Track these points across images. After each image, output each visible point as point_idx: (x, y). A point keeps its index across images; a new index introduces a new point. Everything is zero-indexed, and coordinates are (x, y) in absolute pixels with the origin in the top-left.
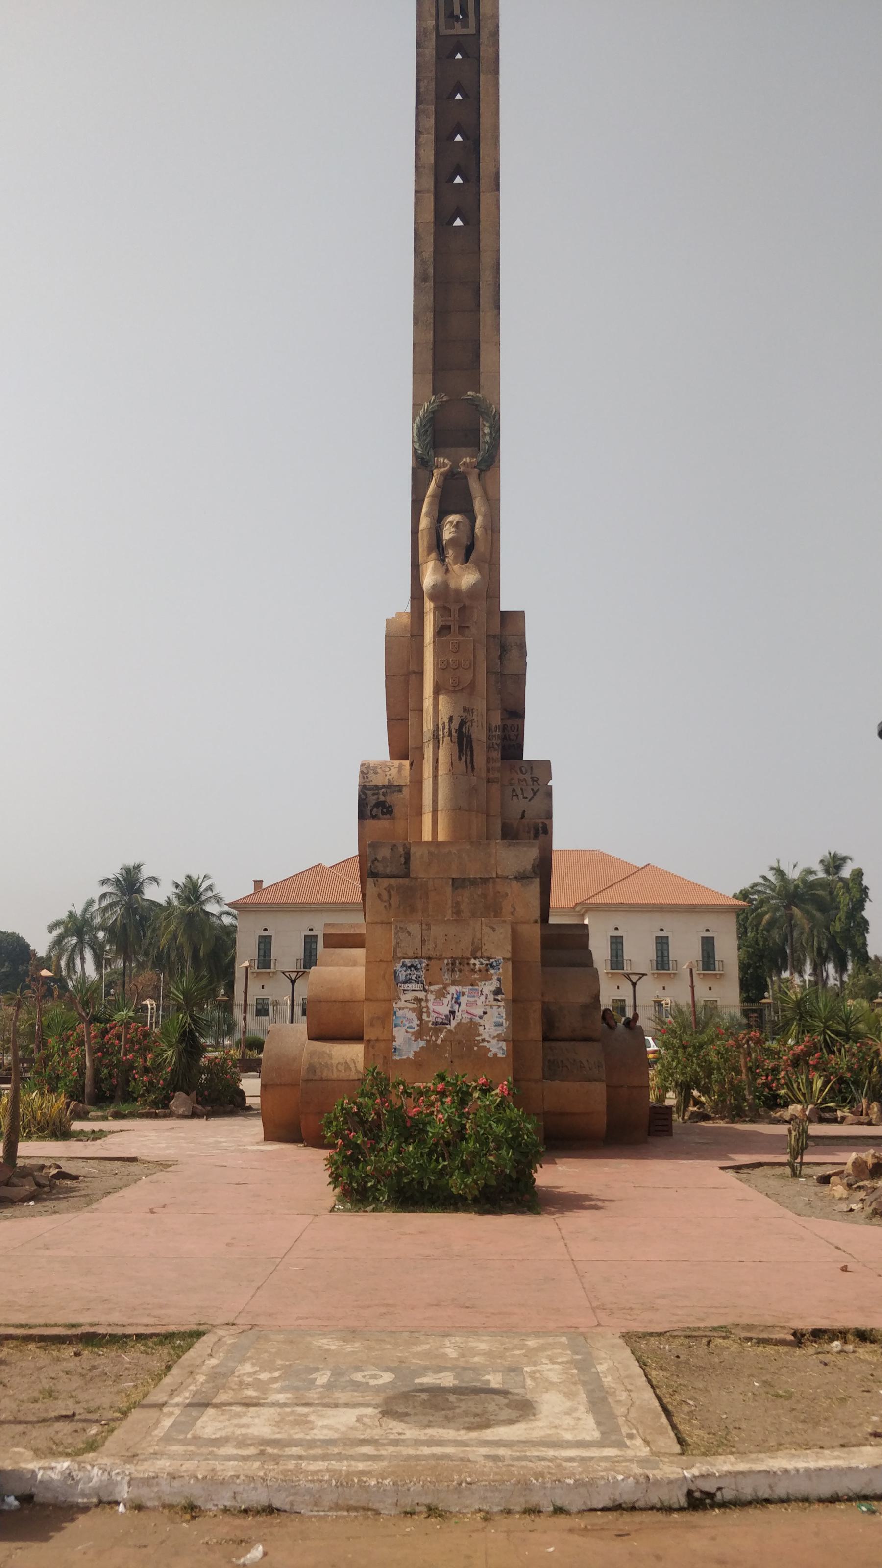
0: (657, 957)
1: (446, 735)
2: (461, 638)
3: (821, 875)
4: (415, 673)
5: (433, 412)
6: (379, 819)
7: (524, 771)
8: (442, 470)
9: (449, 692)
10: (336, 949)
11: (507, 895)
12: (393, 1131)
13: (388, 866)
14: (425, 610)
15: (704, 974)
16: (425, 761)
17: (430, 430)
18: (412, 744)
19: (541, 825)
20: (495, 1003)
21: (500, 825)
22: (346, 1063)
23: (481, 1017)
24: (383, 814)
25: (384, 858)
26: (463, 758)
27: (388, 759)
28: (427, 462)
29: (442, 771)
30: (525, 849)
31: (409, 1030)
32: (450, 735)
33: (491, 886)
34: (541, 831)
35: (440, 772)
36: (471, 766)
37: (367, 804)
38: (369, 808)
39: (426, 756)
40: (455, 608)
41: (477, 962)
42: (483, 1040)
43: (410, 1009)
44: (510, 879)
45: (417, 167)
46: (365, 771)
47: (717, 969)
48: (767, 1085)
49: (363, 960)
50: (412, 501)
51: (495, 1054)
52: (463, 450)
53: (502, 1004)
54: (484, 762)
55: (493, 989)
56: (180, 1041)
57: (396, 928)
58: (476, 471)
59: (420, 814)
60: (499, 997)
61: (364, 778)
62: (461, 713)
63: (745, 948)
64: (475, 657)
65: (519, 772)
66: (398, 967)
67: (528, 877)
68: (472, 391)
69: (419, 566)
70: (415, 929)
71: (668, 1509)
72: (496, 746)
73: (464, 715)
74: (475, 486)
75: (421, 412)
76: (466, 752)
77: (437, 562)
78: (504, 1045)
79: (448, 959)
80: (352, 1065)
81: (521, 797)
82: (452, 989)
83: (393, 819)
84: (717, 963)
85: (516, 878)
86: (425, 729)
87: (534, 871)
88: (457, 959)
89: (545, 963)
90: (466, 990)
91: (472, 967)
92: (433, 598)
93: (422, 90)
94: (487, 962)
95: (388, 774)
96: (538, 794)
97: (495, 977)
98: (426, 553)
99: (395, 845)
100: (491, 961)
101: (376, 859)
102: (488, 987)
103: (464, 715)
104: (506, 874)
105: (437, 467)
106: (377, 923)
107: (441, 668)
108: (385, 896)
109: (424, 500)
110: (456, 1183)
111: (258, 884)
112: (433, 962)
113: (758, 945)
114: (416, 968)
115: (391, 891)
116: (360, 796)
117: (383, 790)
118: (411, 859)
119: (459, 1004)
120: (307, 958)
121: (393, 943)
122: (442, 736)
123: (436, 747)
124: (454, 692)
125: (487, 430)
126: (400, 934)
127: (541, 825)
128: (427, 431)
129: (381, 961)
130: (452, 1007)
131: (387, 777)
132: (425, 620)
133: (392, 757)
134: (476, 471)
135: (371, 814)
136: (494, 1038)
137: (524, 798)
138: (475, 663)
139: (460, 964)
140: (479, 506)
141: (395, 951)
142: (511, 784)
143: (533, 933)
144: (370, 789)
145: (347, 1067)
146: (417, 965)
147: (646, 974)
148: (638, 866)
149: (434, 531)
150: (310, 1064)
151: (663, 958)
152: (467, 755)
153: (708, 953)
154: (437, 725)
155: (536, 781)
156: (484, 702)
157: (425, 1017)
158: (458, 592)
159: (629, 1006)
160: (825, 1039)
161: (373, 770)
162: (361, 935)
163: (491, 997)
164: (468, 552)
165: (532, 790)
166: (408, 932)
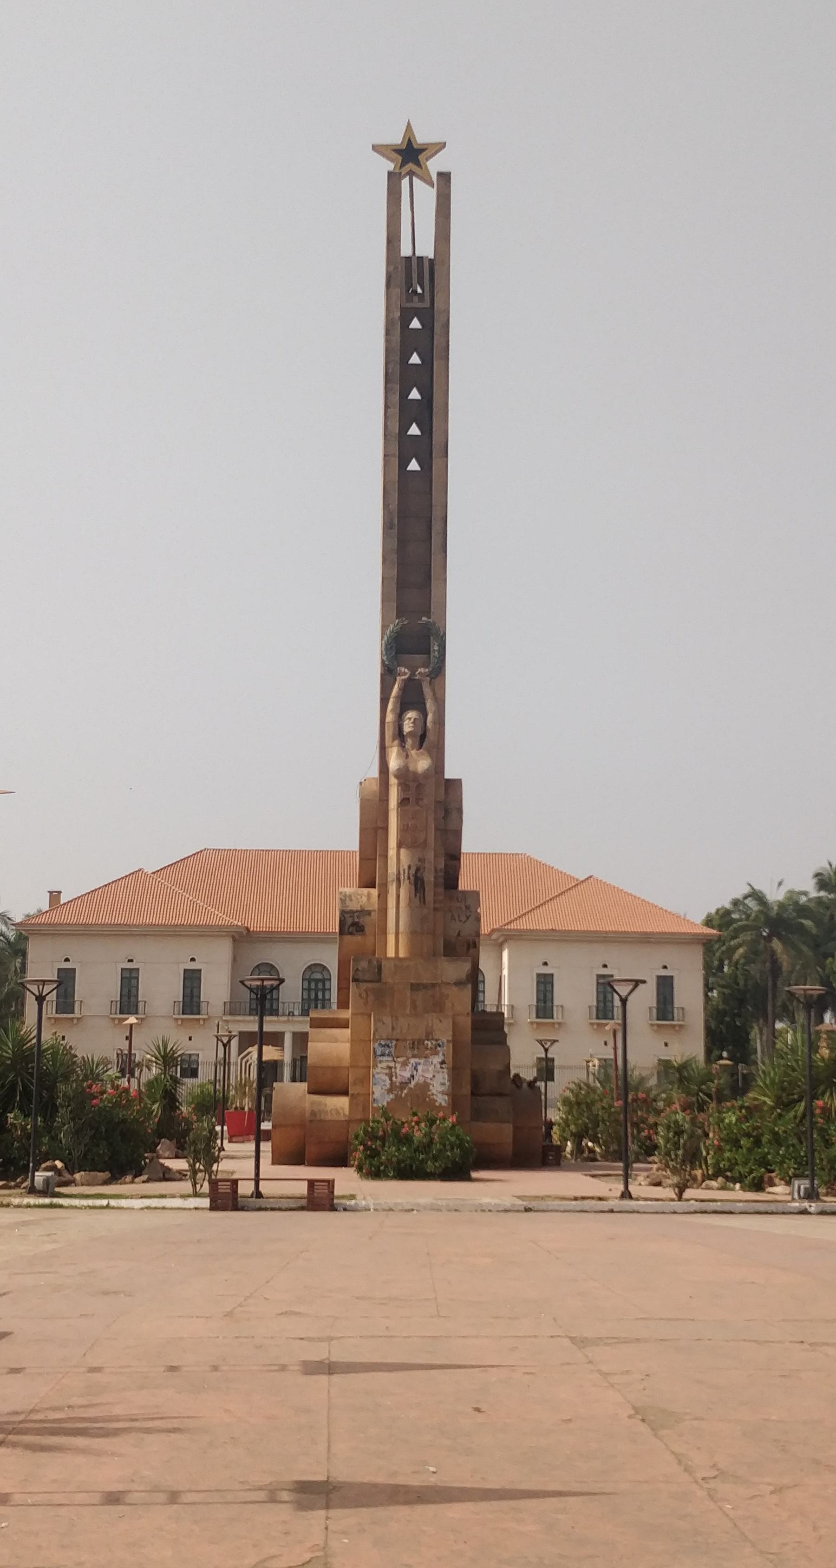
0: (598, 1001)
1: (406, 877)
2: (417, 808)
3: (814, 894)
4: (382, 828)
6: (354, 935)
8: (403, 677)
9: (408, 847)
10: (323, 1030)
12: (394, 1141)
15: (659, 1026)
16: (389, 896)
20: (440, 1070)
22: (337, 1110)
23: (431, 1079)
24: (357, 931)
31: (384, 1087)
32: (409, 878)
36: (423, 900)
38: (347, 927)
40: (413, 785)
41: (429, 1043)
42: (433, 1094)
43: (384, 1073)
45: (385, 435)
46: (343, 898)
47: (676, 1018)
48: (649, 1138)
51: (441, 1104)
53: (445, 1070)
55: (440, 1060)
56: (164, 1097)
58: (428, 678)
60: (444, 1066)
63: (720, 989)
66: (376, 1045)
70: (388, 1020)
71: (518, 1211)
73: (419, 863)
74: (427, 690)
78: (446, 1098)
80: (341, 1111)
82: (413, 1061)
83: (364, 935)
84: (676, 1010)
86: (389, 871)
89: (474, 1041)
90: (422, 1061)
91: (426, 1046)
92: (396, 776)
93: (390, 371)
95: (360, 901)
96: (470, 918)
97: (441, 1054)
101: (357, 969)
102: (437, 1060)
104: (448, 981)
105: (399, 675)
107: (403, 830)
108: (364, 995)
110: (430, 1166)
111: (54, 896)
113: (738, 984)
114: (388, 1046)
119: (417, 1071)
120: (125, 999)
122: (402, 878)
125: (436, 648)
127: (471, 940)
128: (391, 647)
130: (412, 1072)
134: (428, 678)
136: (440, 1093)
140: (430, 705)
143: (466, 1022)
145: (338, 1112)
147: (644, 982)
148: (577, 876)
149: (397, 724)
150: (312, 1110)
151: (605, 1003)
153: (665, 998)
154: (399, 872)
157: (394, 1079)
158: (415, 773)
159: (226, 1139)
160: (698, 1099)
163: (438, 1066)
164: (422, 738)
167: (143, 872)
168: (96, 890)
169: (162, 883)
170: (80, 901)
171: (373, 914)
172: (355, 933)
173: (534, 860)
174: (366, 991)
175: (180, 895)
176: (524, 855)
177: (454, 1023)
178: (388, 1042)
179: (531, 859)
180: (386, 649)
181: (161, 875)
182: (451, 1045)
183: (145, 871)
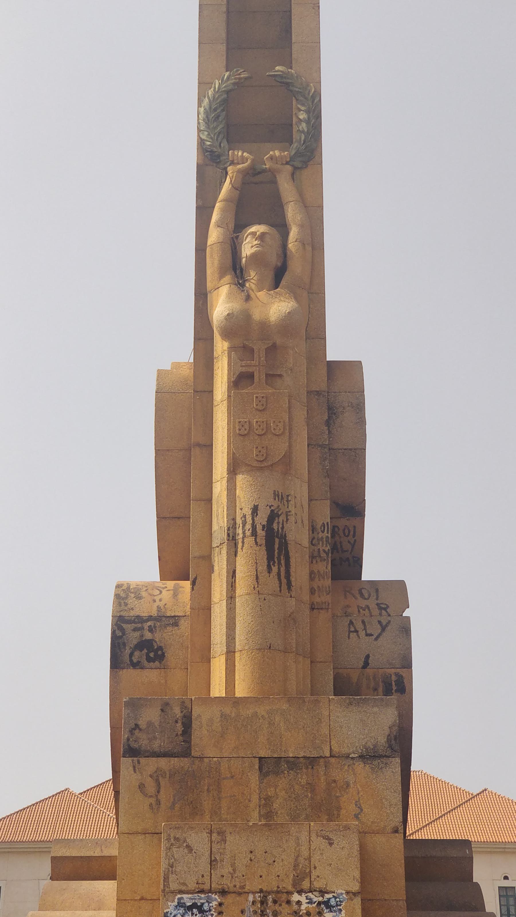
1: (248, 533)
4: (198, 445)
5: (228, 92)
7: (366, 596)
8: (240, 166)
9: (252, 469)
11: (348, 785)
13: (155, 738)
16: (215, 576)
18: (194, 551)
19: (394, 678)
21: (332, 677)
25: (150, 724)
26: (275, 569)
28: (219, 156)
30: (376, 709)
32: (254, 533)
33: (321, 770)
34: (394, 688)
35: (239, 591)
37: (124, 644)
38: (128, 651)
39: (216, 568)
40: (260, 348)
41: (303, 898)
46: (123, 595)
49: (112, 901)
50: (198, 208)
52: (269, 145)
54: (307, 577)
57: (168, 839)
58: (289, 168)
61: (120, 606)
62: (271, 502)
65: (358, 596)
67: (381, 757)
68: (279, 65)
72: (323, 555)
73: (275, 504)
75: (210, 92)
79: (254, 893)
81: (362, 633)
87: (390, 746)
88: (269, 893)
91: (295, 907)
94: (321, 899)
95: (157, 598)
98: (217, 275)
99: (167, 704)
100: (327, 896)
101: (137, 726)
103: (275, 504)
105: (232, 163)
106: (137, 833)
108: (151, 787)
109: (214, 207)
112: (229, 899)
115: (160, 779)
116: (113, 633)
117: (149, 623)
118: (193, 725)
121: (164, 865)
122: (241, 536)
123: (233, 553)
124: (261, 469)
125: (302, 116)
127: (394, 678)
128: (218, 117)
129: (142, 899)
131: (156, 604)
132: (215, 368)
133: (163, 577)
134: (289, 168)
135: (131, 660)
137: (367, 635)
139: (275, 902)
141: (166, 879)
142: (347, 614)
144: (129, 622)
146: (203, 904)
152: (279, 563)
154: (234, 519)
155: (385, 609)
156: (305, 488)
158: (264, 325)
161: (135, 593)
162: (111, 859)
165: (380, 622)
166: (188, 846)
170: (8, 820)
171: (182, 622)
172: (145, 663)
173: (431, 777)
174: (156, 776)
177: (362, 849)
178: (201, 899)
180: (207, 120)
182: (358, 901)
183: (70, 791)
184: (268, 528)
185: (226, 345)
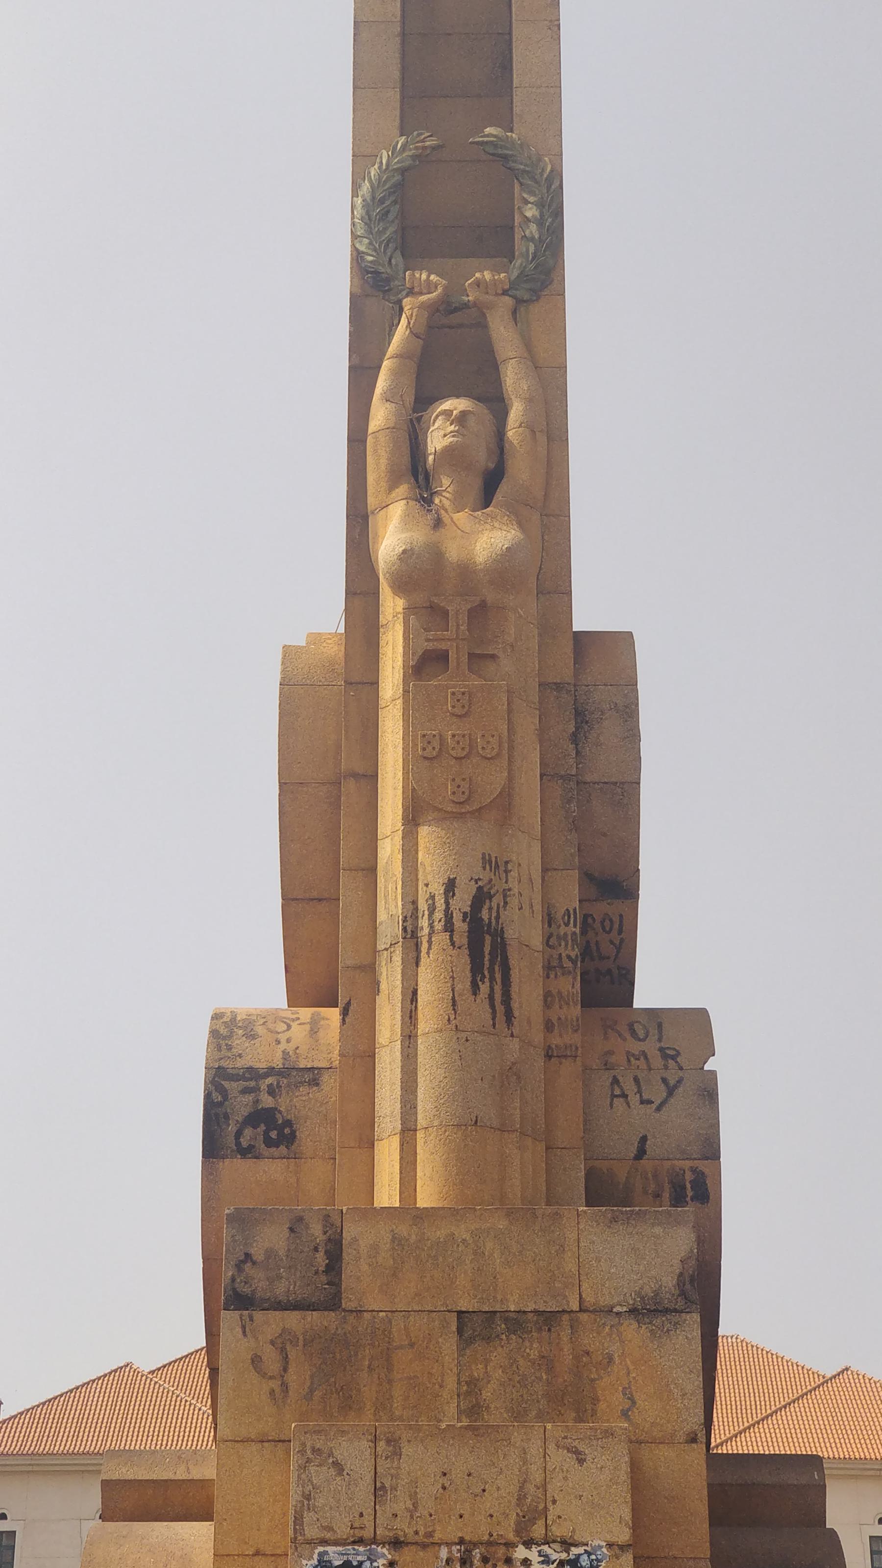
1: (438, 926)
4: (355, 775)
5: (403, 171)
7: (641, 1034)
9: (445, 817)
11: (610, 1360)
14: (382, 620)
16: (381, 1000)
17: (395, 210)
18: (346, 957)
19: (689, 1176)
24: (269, 1143)
25: (270, 1253)
26: (484, 988)
27: (284, 1005)
28: (388, 280)
29: (427, 1021)
30: (658, 1230)
32: (449, 927)
33: (565, 1335)
34: (690, 1193)
37: (226, 1117)
38: (232, 1128)
39: (383, 986)
40: (458, 608)
44: (618, 1314)
46: (223, 1031)
50: (351, 369)
57: (302, 1452)
58: (508, 301)
59: (368, 1143)
61: (219, 1050)
62: (478, 871)
64: (511, 730)
65: (628, 1035)
67: (667, 1311)
69: (365, 518)
72: (568, 964)
73: (486, 876)
75: (374, 171)
76: (492, 971)
77: (413, 503)
79: (449, 1545)
81: (634, 1099)
85: (633, 1311)
87: (683, 1294)
88: (475, 1545)
94: (564, 1556)
95: (283, 1038)
99: (300, 1219)
100: (575, 1551)
103: (486, 876)
104: (605, 1300)
105: (411, 292)
108: (271, 1360)
109: (380, 367)
116: (208, 1096)
117: (269, 1080)
121: (295, 1495)
122: (426, 931)
123: (413, 961)
124: (460, 816)
125: (531, 212)
126: (312, 1469)
127: (689, 1176)
129: (257, 1553)
132: (382, 643)
134: (508, 301)
135: (238, 1144)
137: (642, 1102)
138: (511, 748)
141: (298, 1520)
152: (492, 979)
154: (415, 902)
155: (673, 1058)
156: (537, 847)
158: (466, 570)
161: (245, 1028)
162: (204, 1484)
165: (664, 1081)
166: (336, 1464)
167: (131, 1368)
168: (55, 1398)
169: (160, 1386)
175: (188, 1403)
176: (737, 1338)
177: (635, 1467)
179: (747, 1343)
180: (368, 220)
181: (164, 1376)
183: (134, 1367)
184: (473, 917)
185: (400, 604)
